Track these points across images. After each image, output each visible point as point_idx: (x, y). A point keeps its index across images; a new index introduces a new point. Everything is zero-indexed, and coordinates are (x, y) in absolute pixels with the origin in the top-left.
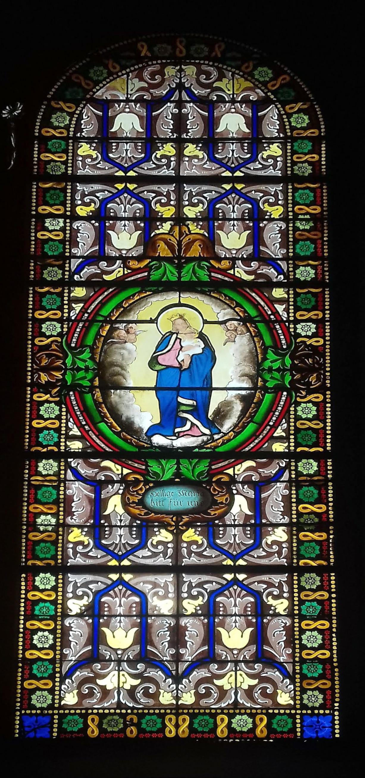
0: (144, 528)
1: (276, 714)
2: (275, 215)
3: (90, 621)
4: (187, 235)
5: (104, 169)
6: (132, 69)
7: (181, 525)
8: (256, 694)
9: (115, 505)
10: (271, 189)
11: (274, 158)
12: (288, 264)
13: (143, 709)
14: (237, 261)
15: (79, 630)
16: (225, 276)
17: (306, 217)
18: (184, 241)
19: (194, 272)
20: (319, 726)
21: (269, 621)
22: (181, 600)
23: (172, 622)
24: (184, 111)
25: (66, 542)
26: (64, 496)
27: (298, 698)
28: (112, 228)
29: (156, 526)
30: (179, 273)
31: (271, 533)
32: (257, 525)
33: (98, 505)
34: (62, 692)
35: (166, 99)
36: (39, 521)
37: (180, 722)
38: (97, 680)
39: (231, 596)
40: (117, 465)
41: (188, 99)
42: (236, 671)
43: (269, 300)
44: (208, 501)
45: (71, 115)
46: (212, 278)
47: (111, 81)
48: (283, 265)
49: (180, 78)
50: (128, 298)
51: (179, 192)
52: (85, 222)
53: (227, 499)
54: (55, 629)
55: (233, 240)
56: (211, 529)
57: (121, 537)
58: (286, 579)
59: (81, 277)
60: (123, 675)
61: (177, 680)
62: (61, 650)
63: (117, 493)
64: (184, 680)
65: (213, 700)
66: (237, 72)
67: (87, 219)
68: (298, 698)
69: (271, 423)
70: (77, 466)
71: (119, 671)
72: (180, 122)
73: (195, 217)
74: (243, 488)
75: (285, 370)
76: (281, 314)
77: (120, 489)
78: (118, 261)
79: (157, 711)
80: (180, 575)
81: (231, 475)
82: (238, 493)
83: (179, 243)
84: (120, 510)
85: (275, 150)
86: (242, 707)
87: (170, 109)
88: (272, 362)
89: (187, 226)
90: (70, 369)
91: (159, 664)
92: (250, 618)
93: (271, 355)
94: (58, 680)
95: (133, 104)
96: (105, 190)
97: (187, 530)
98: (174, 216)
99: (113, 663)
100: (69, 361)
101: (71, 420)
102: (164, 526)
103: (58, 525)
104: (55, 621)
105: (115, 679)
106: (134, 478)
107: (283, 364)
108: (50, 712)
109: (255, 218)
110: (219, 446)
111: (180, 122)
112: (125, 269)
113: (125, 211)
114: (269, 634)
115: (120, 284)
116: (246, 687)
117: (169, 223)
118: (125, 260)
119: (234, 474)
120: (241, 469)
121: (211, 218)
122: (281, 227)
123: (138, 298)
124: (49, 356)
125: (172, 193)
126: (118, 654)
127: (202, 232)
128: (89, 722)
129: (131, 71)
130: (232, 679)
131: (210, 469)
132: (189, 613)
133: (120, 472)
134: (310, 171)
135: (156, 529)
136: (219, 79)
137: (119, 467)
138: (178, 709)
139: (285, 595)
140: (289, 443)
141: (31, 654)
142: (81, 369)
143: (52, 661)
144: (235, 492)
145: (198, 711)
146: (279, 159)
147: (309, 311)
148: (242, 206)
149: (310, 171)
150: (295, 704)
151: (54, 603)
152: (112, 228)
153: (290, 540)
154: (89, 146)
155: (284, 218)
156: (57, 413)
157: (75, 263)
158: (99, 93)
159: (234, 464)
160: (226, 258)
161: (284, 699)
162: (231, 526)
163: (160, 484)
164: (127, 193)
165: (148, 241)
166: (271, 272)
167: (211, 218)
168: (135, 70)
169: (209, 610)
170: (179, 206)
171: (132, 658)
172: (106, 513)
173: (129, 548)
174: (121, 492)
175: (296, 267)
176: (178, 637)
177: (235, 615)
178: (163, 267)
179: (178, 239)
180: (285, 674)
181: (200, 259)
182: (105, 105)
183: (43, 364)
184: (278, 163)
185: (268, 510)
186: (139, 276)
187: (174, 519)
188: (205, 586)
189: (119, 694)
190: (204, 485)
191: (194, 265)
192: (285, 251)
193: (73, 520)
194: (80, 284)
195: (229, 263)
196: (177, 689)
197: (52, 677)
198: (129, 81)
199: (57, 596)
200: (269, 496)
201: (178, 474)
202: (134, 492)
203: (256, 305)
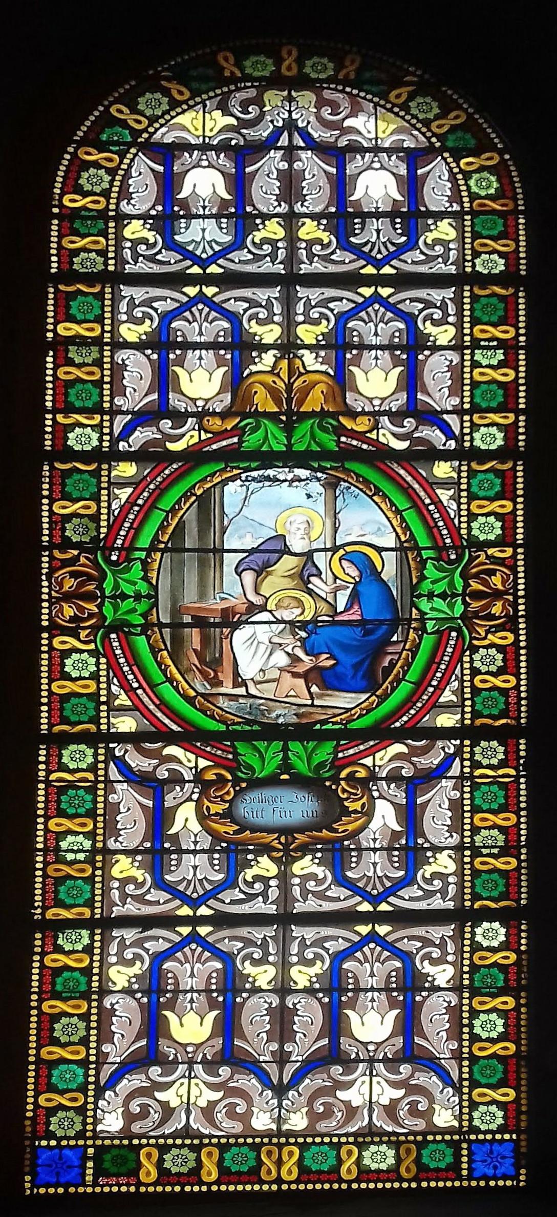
0: (233, 853)
1: (232, 1145)
2: (443, 340)
3: (145, 1000)
4: (301, 374)
5: (343, 262)
6: (211, 94)
7: (292, 850)
8: (401, 1112)
9: (185, 819)
10: (262, 296)
11: (273, 243)
12: (462, 422)
13: (406, 1135)
14: (192, 778)
15: (126, 1014)
16: (363, 442)
17: (491, 344)
18: (295, 385)
19: (313, 437)
20: (56, 1167)
21: (245, 1000)
22: (287, 967)
23: (275, 1001)
24: (297, 165)
25: (107, 878)
26: (105, 805)
27: (466, 1117)
28: (180, 362)
29: (250, 851)
30: (286, 758)
31: (252, 863)
32: (411, 850)
33: (159, 819)
34: (99, 1111)
35: (270, 143)
36: (64, 845)
37: (285, 1157)
38: (338, 1092)
39: (187, 961)
40: (188, 754)
41: (303, 145)
42: (371, 1075)
43: (427, 481)
44: (333, 810)
45: (112, 172)
46: (342, 445)
47: (178, 114)
48: (453, 421)
49: (290, 112)
50: (204, 480)
51: (288, 302)
52: (136, 352)
53: (363, 805)
54: (88, 1014)
55: (376, 382)
56: (337, 856)
57: (195, 869)
58: (452, 933)
59: (130, 446)
60: (379, 1083)
61: (280, 1091)
62: (98, 1048)
63: (189, 799)
64: (291, 1093)
65: (335, 1123)
66: (382, 102)
67: (139, 346)
68: (466, 1117)
69: (434, 683)
70: (124, 756)
71: (190, 1078)
72: (290, 186)
73: (314, 342)
74: (389, 788)
75: (454, 595)
76: (446, 504)
77: (193, 792)
78: (190, 420)
79: (249, 1141)
80: (288, 927)
81: (369, 768)
82: (381, 797)
83: (289, 387)
84: (195, 826)
85: (445, 230)
86: (197, 1133)
87: (274, 160)
88: (433, 582)
89: (300, 358)
90: (458, 595)
91: (252, 1066)
92: (395, 994)
93: (431, 571)
94: (91, 1093)
95: (385, 154)
96: (343, 298)
97: (302, 858)
98: (279, 341)
99: (361, 1065)
100: (108, 586)
101: (115, 680)
102: (266, 849)
103: (94, 851)
104: (90, 1001)
105: (368, 1092)
106: (215, 774)
107: (451, 584)
108: (81, 1142)
109: (412, 349)
110: (354, 720)
111: (290, 186)
112: (202, 432)
113: (376, 334)
114: (245, 1021)
115: (194, 457)
116: (204, 1104)
117: (272, 352)
118: (201, 415)
119: (374, 766)
120: (386, 757)
121: (341, 346)
122: (451, 361)
123: (219, 479)
124: (74, 575)
125: (448, 302)
126: (188, 1053)
127: (323, 368)
128: (264, 1157)
129: (210, 98)
130: (183, 1091)
131: (336, 758)
132: (300, 986)
133: (193, 764)
134: (503, 268)
135: (250, 857)
136: (353, 114)
137: (192, 757)
138: (280, 1136)
139: (450, 958)
140: (463, 713)
141: (50, 1053)
142: (438, 596)
143: (84, 1063)
144: (376, 794)
145: (409, 1138)
146: (280, 244)
147: (491, 500)
148: (213, 324)
149: (503, 268)
150: (461, 1126)
151: (87, 972)
152: (180, 362)
153: (459, 872)
154: (316, 223)
155: (457, 346)
156: (93, 668)
157: (120, 422)
158: (158, 135)
159: (373, 750)
160: (363, 413)
161: (444, 1118)
162: (188, 851)
163: (257, 784)
164: (379, 304)
165: (236, 381)
166: (436, 436)
167: (341, 346)
168: (217, 95)
169: (225, 984)
170: (292, 239)
171: (209, 1058)
172: (172, 831)
173: (388, 884)
174: (195, 797)
175: (474, 427)
176: (282, 1023)
177: (372, 989)
178: (263, 428)
179: (286, 381)
180: (446, 1078)
181: (323, 414)
182: (165, 154)
183: (66, 588)
184: (280, 251)
185: (148, 373)
186: (224, 443)
187: (283, 839)
188: (326, 945)
189: (188, 1113)
190: (327, 783)
191: (314, 422)
192: (458, 400)
193: (118, 843)
194: (127, 457)
195: (369, 420)
196: (280, 1106)
197: (83, 1089)
198: (207, 115)
199: (92, 961)
200: (429, 800)
201: (286, 765)
202: (216, 797)
203: (407, 490)
